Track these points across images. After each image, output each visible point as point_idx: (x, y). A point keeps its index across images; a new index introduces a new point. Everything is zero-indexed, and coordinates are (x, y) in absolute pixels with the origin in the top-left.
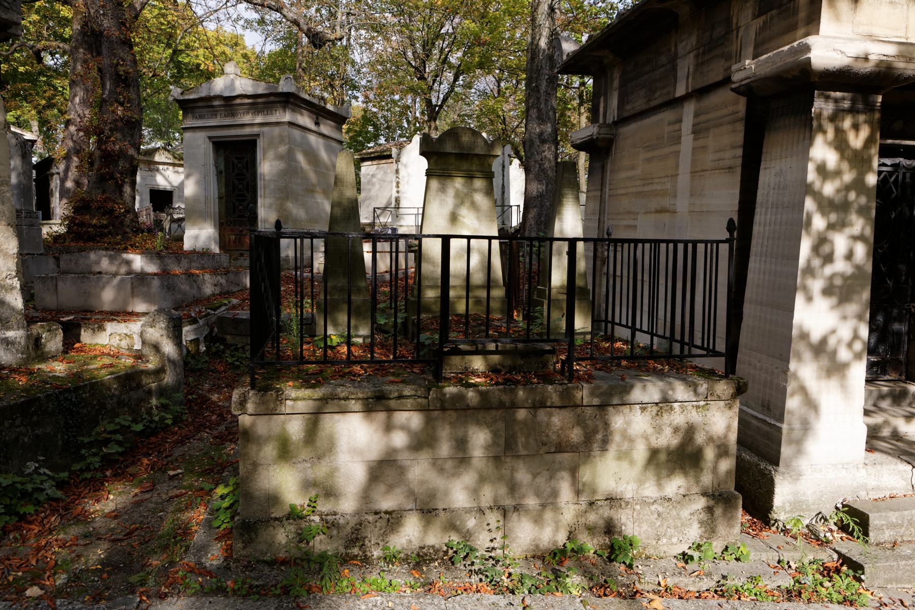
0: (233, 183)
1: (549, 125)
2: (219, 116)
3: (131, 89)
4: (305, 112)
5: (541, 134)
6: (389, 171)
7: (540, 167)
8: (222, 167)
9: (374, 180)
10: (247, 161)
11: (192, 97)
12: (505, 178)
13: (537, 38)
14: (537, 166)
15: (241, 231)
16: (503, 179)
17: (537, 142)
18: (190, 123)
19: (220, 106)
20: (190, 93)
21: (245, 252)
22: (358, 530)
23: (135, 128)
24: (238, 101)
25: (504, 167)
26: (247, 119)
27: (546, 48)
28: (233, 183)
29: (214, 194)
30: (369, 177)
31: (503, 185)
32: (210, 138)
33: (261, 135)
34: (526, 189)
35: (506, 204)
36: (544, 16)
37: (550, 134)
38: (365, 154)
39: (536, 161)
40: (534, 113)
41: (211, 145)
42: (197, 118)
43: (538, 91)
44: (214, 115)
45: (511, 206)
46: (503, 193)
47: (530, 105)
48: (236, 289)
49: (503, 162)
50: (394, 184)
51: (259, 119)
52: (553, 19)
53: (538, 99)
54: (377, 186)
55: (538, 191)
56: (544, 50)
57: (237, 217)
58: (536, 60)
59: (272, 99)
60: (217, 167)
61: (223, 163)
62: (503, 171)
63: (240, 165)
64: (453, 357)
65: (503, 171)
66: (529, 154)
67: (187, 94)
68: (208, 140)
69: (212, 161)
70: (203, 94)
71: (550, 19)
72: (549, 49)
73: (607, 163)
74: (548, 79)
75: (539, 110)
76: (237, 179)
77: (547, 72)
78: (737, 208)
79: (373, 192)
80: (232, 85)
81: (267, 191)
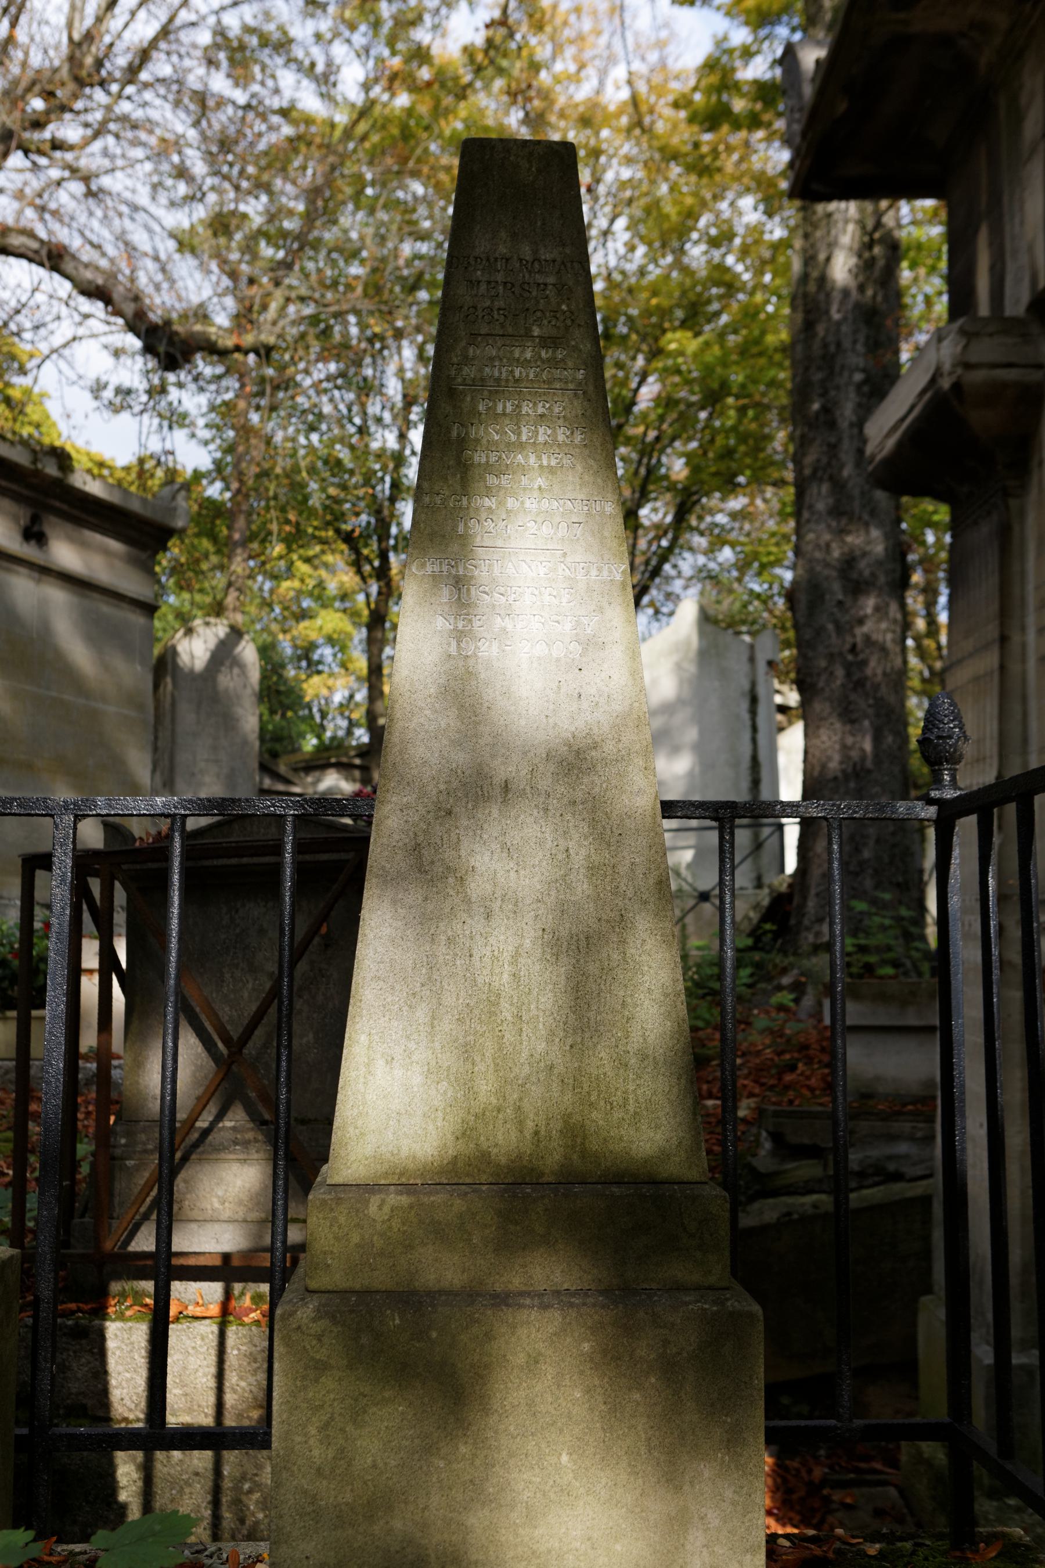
1: (875, 533)
5: (849, 561)
7: (848, 675)
13: (822, 257)
14: (840, 672)
16: (754, 741)
17: (836, 590)
27: (853, 284)
31: (755, 763)
37: (880, 563)
39: (831, 657)
40: (821, 497)
43: (832, 425)
47: (807, 472)
49: (753, 685)
53: (833, 449)
55: (846, 758)
56: (846, 292)
58: (821, 329)
66: (808, 634)
72: (861, 288)
73: (1022, 513)
74: (865, 382)
75: (838, 486)
77: (861, 362)
78: (1030, 1184)
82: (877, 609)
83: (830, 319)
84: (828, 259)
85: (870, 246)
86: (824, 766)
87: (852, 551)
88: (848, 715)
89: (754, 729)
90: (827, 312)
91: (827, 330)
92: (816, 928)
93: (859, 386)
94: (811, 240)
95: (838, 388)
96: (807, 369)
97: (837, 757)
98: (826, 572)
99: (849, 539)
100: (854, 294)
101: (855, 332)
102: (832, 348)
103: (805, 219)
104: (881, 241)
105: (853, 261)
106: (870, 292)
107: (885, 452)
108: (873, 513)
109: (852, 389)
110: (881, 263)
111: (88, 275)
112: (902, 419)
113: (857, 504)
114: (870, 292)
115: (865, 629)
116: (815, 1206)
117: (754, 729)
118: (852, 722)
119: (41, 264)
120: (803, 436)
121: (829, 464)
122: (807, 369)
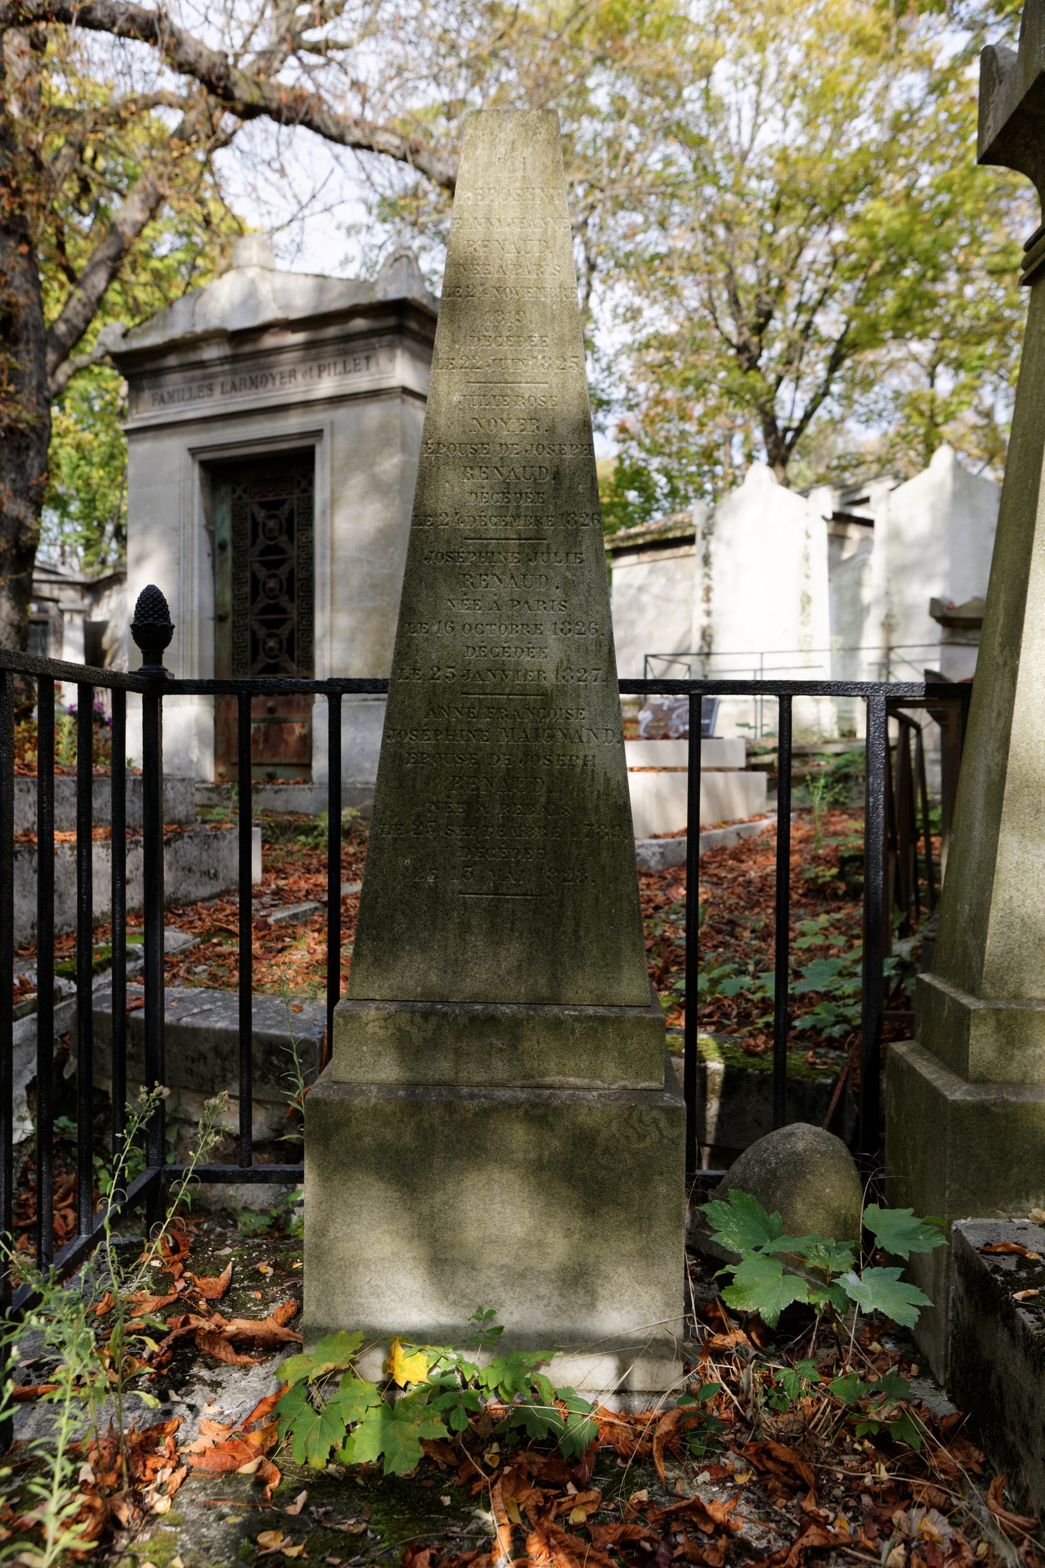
0: (254, 576)
2: (218, 390)
3: (21, 347)
6: (678, 576)
8: (225, 533)
9: (645, 598)
10: (291, 513)
15: (271, 711)
18: (148, 414)
19: (223, 360)
20: (145, 333)
21: (279, 771)
23: (28, 448)
24: (270, 341)
26: (295, 390)
28: (254, 576)
29: (201, 607)
30: (632, 592)
32: (193, 452)
33: (327, 434)
38: (622, 539)
41: (196, 471)
42: (162, 400)
48: (205, 891)
50: (699, 593)
51: (327, 386)
54: (651, 613)
57: (263, 671)
59: (359, 324)
60: (212, 534)
61: (228, 523)
63: (271, 524)
67: (136, 335)
68: (188, 458)
69: (197, 515)
70: (178, 329)
76: (263, 564)
79: (641, 629)
80: (250, 298)
81: (341, 592)
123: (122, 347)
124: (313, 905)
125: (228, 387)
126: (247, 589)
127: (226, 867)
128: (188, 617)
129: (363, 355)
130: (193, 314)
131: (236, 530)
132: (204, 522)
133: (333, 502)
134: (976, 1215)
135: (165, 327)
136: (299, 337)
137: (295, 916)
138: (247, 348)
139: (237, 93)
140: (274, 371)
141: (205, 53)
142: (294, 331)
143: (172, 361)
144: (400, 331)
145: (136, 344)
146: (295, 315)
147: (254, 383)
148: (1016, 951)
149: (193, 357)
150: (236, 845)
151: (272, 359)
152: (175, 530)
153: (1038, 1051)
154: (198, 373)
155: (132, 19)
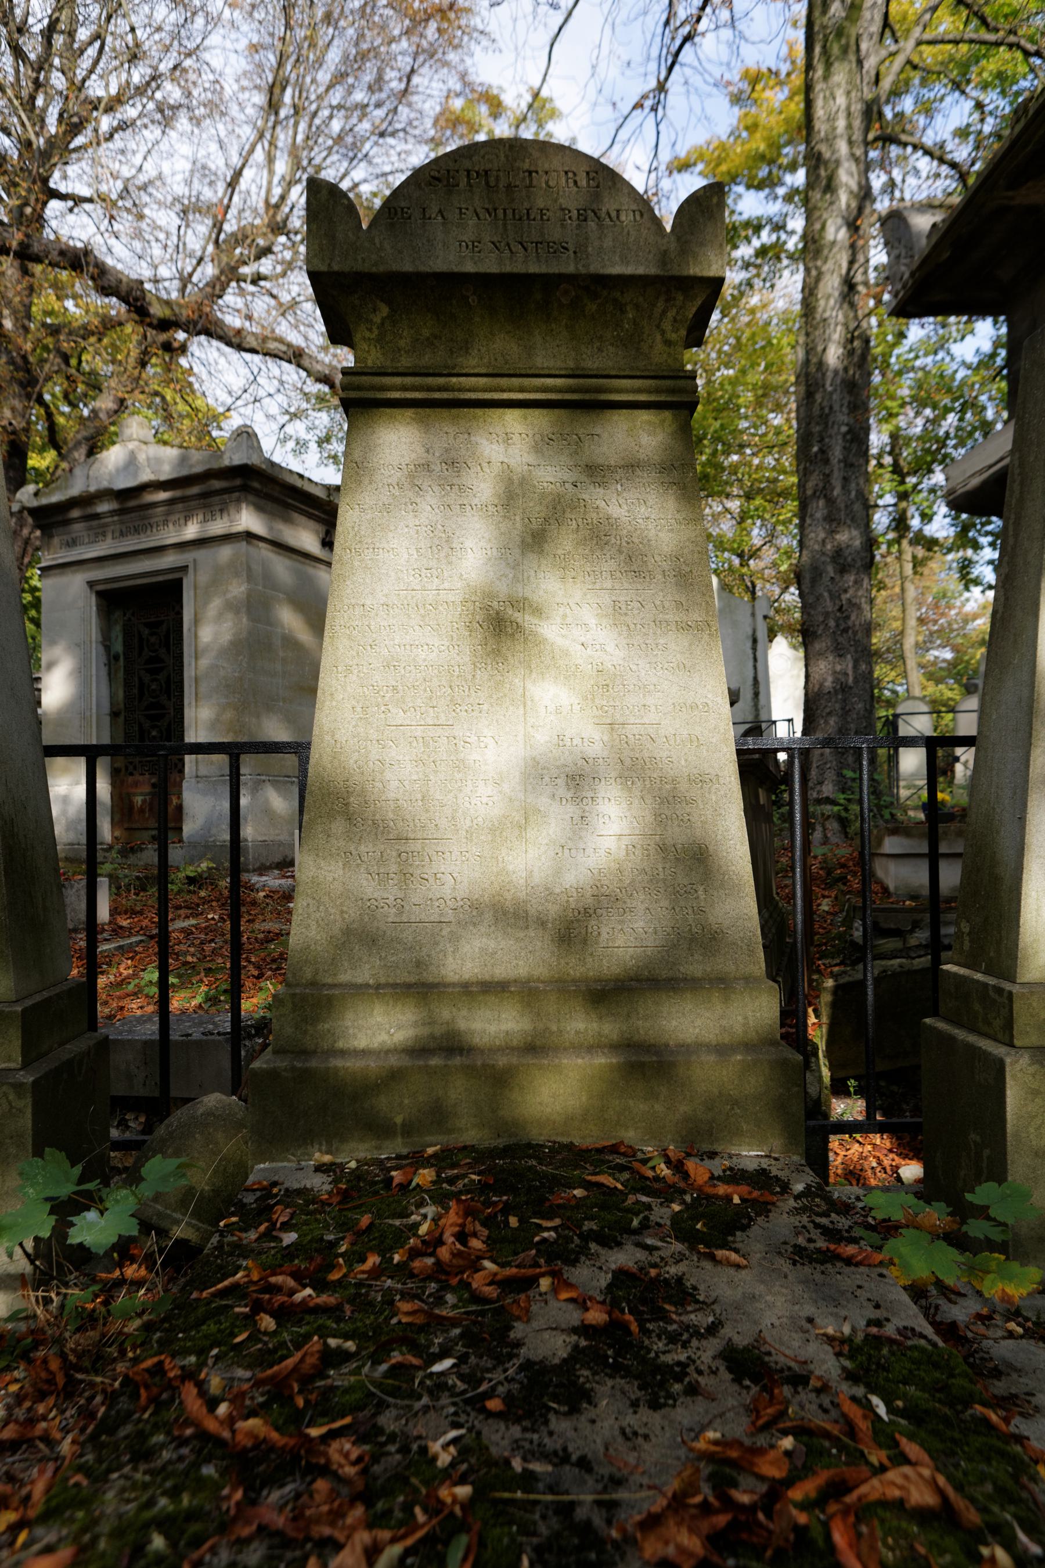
0: (140, 679)
2: (109, 536)
4: (302, 519)
5: (838, 552)
8: (118, 647)
11: (55, 498)
12: (759, 665)
13: (820, 348)
16: (755, 667)
17: (830, 570)
19: (112, 513)
20: (50, 494)
22: (858, 1180)
25: (755, 641)
26: (170, 535)
27: (840, 367)
28: (140, 679)
31: (756, 679)
32: (91, 584)
33: (191, 570)
34: (807, 676)
35: (763, 717)
36: (832, 302)
43: (827, 461)
44: (99, 534)
45: (774, 722)
46: (756, 694)
47: (809, 492)
49: (754, 631)
51: (192, 531)
52: (852, 305)
53: (827, 477)
58: (818, 397)
60: (107, 648)
61: (120, 639)
62: (754, 649)
63: (153, 639)
64: (170, 859)
65: (754, 649)
66: (811, 599)
67: (46, 494)
68: (86, 587)
70: (75, 490)
71: (846, 306)
72: (846, 369)
74: (848, 432)
75: (830, 501)
82: (856, 582)
83: (825, 390)
84: (824, 350)
85: (851, 341)
86: (821, 685)
87: (839, 544)
88: (839, 652)
89: (755, 660)
90: (823, 386)
91: (823, 398)
92: (818, 788)
93: (845, 435)
94: (812, 337)
95: (830, 436)
96: (808, 424)
97: (830, 679)
98: (823, 559)
99: (838, 537)
100: (841, 372)
101: (842, 399)
102: (827, 410)
103: (806, 323)
104: (859, 337)
105: (841, 351)
106: (851, 372)
107: (969, 487)
108: (853, 519)
109: (840, 437)
110: (859, 352)
111: (319, 367)
112: (990, 467)
113: (842, 514)
114: (851, 372)
115: (848, 596)
116: (901, 966)
117: (755, 660)
118: (840, 656)
119: (290, 362)
120: (805, 469)
121: (824, 488)
122: (808, 424)
123: (35, 503)
124: (140, 938)
125: (117, 534)
126: (136, 691)
127: (74, 910)
128: (88, 714)
129: (217, 508)
130: (88, 477)
131: (127, 644)
132: (100, 639)
133: (196, 622)
134: (272, 1160)
135: (66, 488)
136: (163, 496)
137: (121, 947)
138: (132, 503)
139: (152, 311)
140: (152, 521)
141: (124, 280)
142: (165, 490)
143: (75, 513)
144: (245, 489)
145: (44, 501)
146: (163, 477)
147: (137, 531)
148: (313, 947)
149: (90, 511)
150: (83, 893)
151: (150, 511)
152: (78, 645)
153: (326, 1026)
154: (95, 523)
155: (62, 253)
